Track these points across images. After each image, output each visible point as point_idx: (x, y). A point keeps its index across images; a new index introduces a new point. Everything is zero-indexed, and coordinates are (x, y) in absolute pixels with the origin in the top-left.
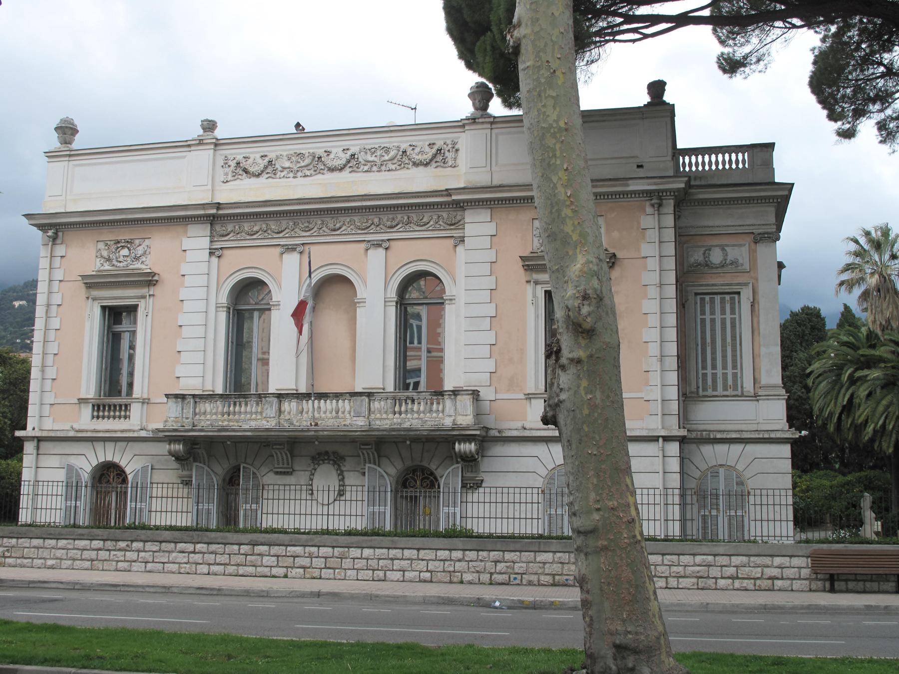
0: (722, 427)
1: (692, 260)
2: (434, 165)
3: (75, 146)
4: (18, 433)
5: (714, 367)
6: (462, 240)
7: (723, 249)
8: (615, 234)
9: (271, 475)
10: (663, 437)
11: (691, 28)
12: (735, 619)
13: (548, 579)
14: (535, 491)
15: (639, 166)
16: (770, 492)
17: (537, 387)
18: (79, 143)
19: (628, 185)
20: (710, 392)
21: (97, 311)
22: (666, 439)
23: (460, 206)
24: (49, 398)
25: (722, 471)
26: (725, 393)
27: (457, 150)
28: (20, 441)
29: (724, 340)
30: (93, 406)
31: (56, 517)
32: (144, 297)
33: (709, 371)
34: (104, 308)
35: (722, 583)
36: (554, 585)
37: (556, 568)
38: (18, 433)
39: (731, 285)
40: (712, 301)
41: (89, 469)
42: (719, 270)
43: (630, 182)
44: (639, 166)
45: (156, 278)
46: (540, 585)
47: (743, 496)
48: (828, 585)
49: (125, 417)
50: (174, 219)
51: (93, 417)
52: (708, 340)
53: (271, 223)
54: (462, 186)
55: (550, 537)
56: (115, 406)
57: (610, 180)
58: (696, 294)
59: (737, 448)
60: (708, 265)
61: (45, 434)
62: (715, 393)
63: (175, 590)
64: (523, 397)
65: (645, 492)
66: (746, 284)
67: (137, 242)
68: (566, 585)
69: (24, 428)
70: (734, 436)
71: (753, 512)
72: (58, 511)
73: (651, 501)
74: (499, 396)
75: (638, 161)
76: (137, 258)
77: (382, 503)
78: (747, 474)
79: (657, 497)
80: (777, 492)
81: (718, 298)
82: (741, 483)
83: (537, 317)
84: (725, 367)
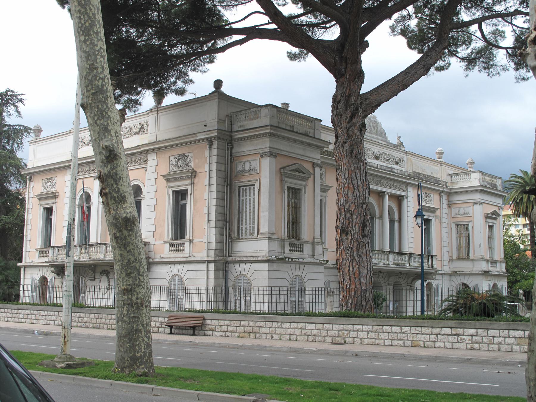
0: (245, 255)
1: (238, 169)
2: (140, 133)
3: (41, 137)
4: (19, 264)
5: (246, 224)
6: (146, 169)
7: (250, 163)
8: (197, 161)
9: (89, 281)
10: (207, 261)
11: (256, 43)
12: (376, 363)
13: (92, 325)
14: (286, 289)
15: (206, 126)
16: (320, 289)
17: (168, 237)
18: (43, 135)
19: (197, 137)
20: (244, 237)
21: (42, 209)
22: (209, 262)
23: (146, 152)
24: (28, 250)
25: (242, 277)
26: (250, 237)
27: (148, 126)
28: (20, 268)
29: (250, 210)
30: (170, 245)
31: (265, 308)
32: (54, 203)
33: (252, 226)
34: (44, 208)
35: (220, 334)
36: (94, 328)
37: (94, 320)
38: (19, 264)
39: (251, 181)
40: (246, 189)
41: (38, 279)
42: (248, 174)
43: (197, 135)
44: (206, 126)
45: (57, 194)
46: (22, 322)
47: (250, 290)
48: (192, 332)
49: (300, 251)
50: (62, 167)
51: (170, 251)
52: (244, 210)
53: (91, 166)
54: (147, 142)
55: (94, 307)
56: (179, 244)
57: (190, 135)
58: (240, 187)
59: (248, 265)
60: (243, 171)
61: (27, 265)
62: (246, 237)
63: (267, 349)
64: (163, 242)
65: (311, 289)
66: (256, 180)
67: (53, 178)
68: (97, 328)
69: (21, 262)
70: (245, 259)
71: (308, 299)
72: (286, 304)
73: (278, 293)
74: (157, 243)
75: (205, 123)
76: (53, 186)
77: (294, 296)
78: (252, 279)
79: (286, 292)
80: (317, 289)
81: (248, 188)
82: (249, 283)
83: (169, 204)
84: (250, 224)
